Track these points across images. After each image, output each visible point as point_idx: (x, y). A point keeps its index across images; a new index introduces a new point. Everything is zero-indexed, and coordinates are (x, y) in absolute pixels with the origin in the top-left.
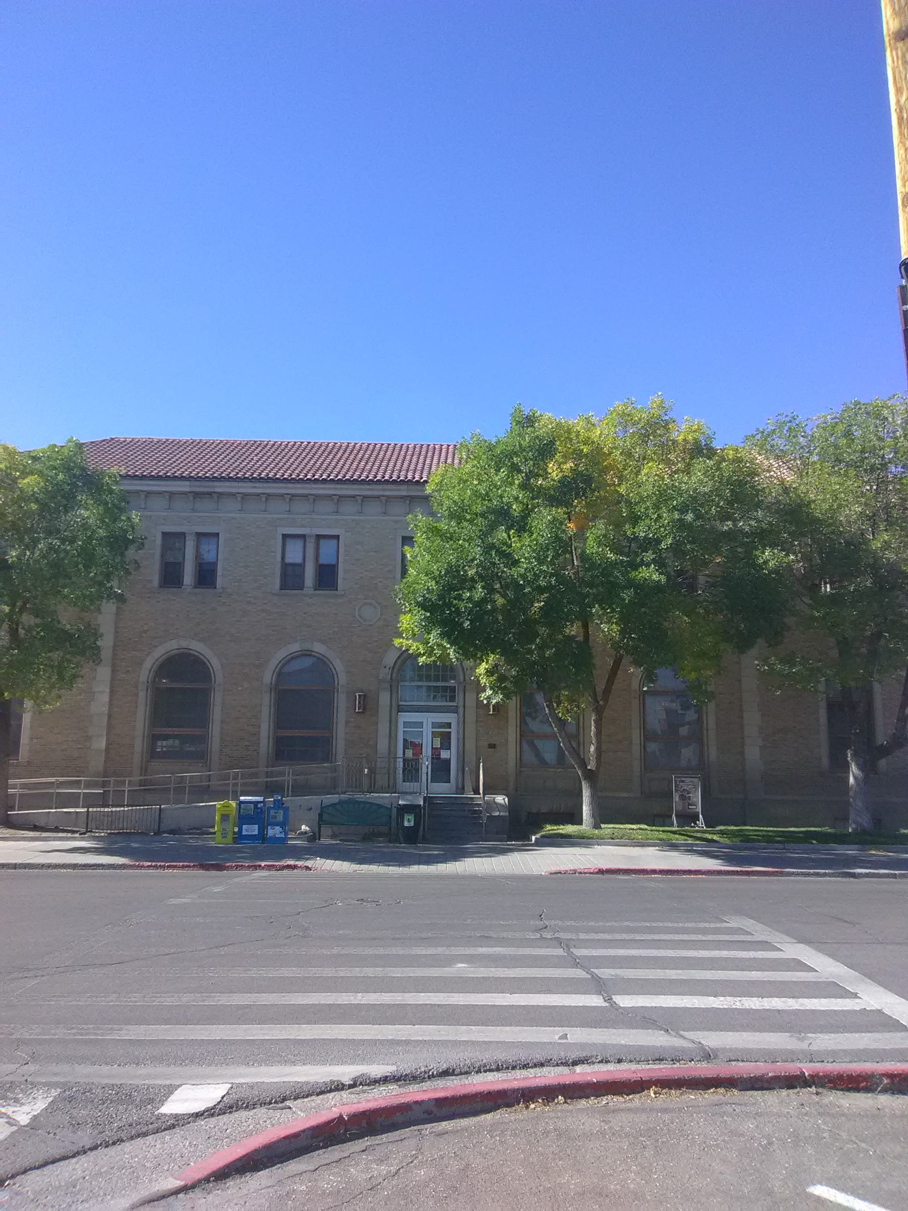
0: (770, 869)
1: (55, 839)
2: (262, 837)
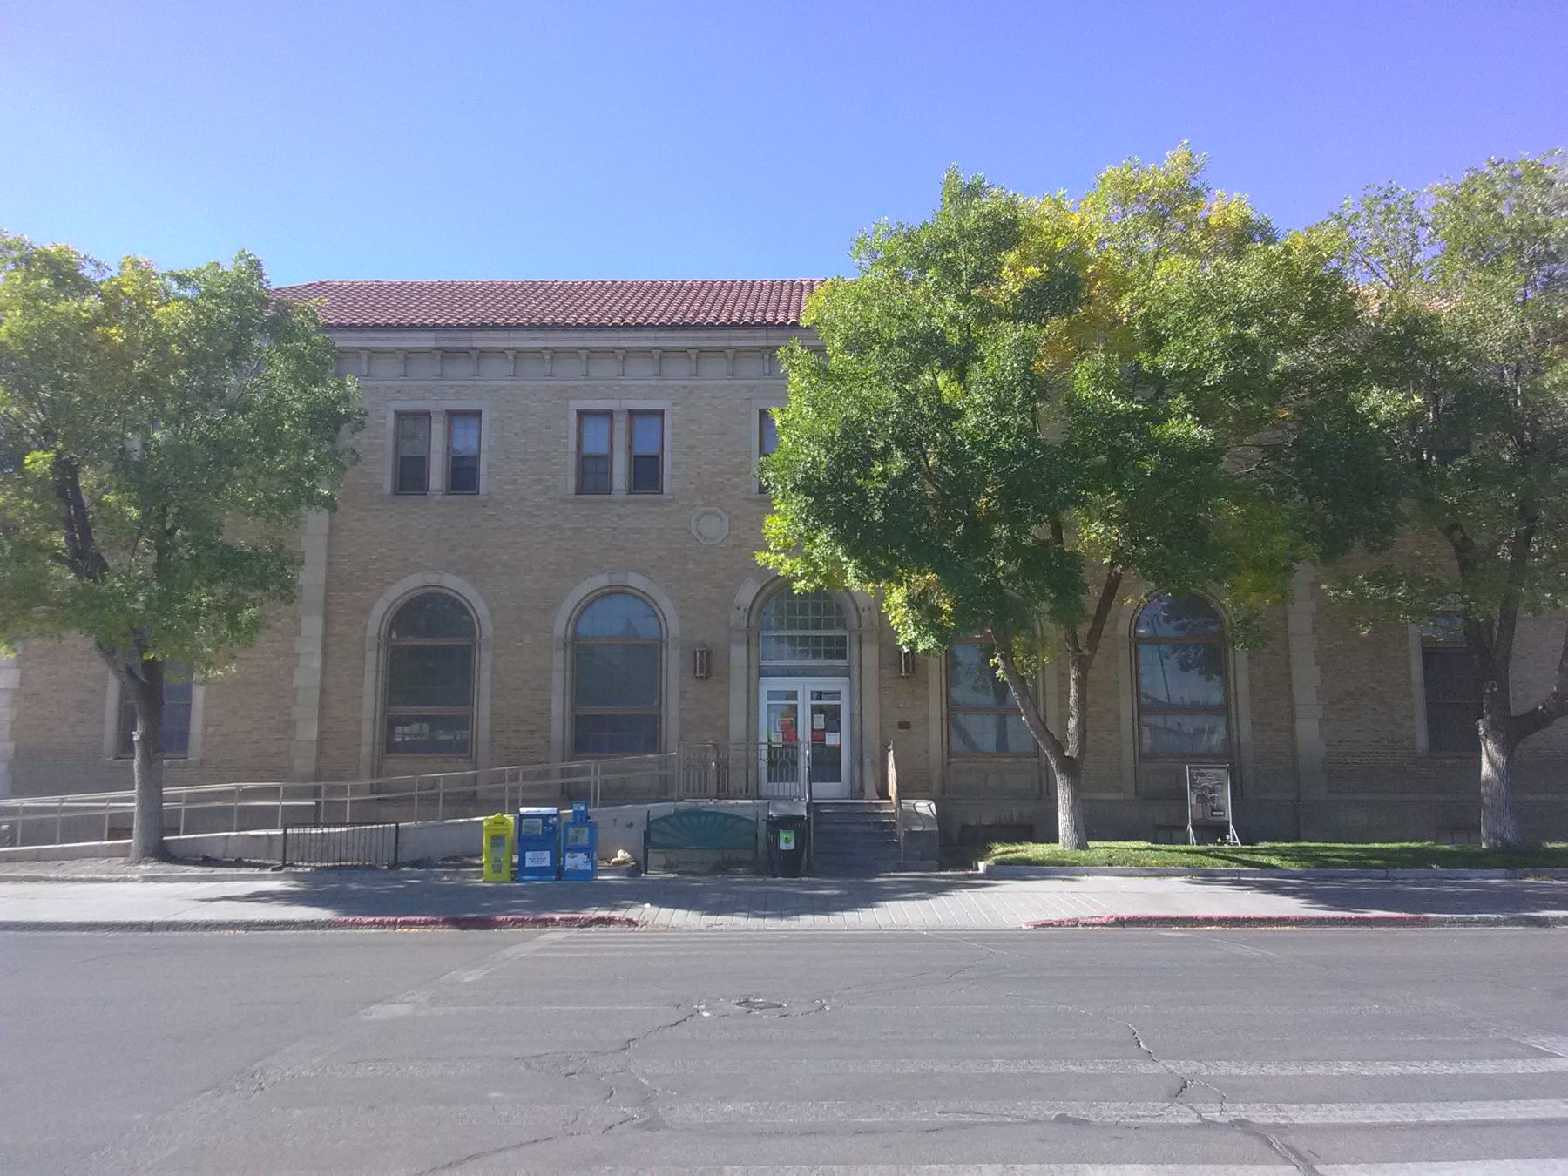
0: (1403, 915)
1: (233, 878)
2: (557, 870)
